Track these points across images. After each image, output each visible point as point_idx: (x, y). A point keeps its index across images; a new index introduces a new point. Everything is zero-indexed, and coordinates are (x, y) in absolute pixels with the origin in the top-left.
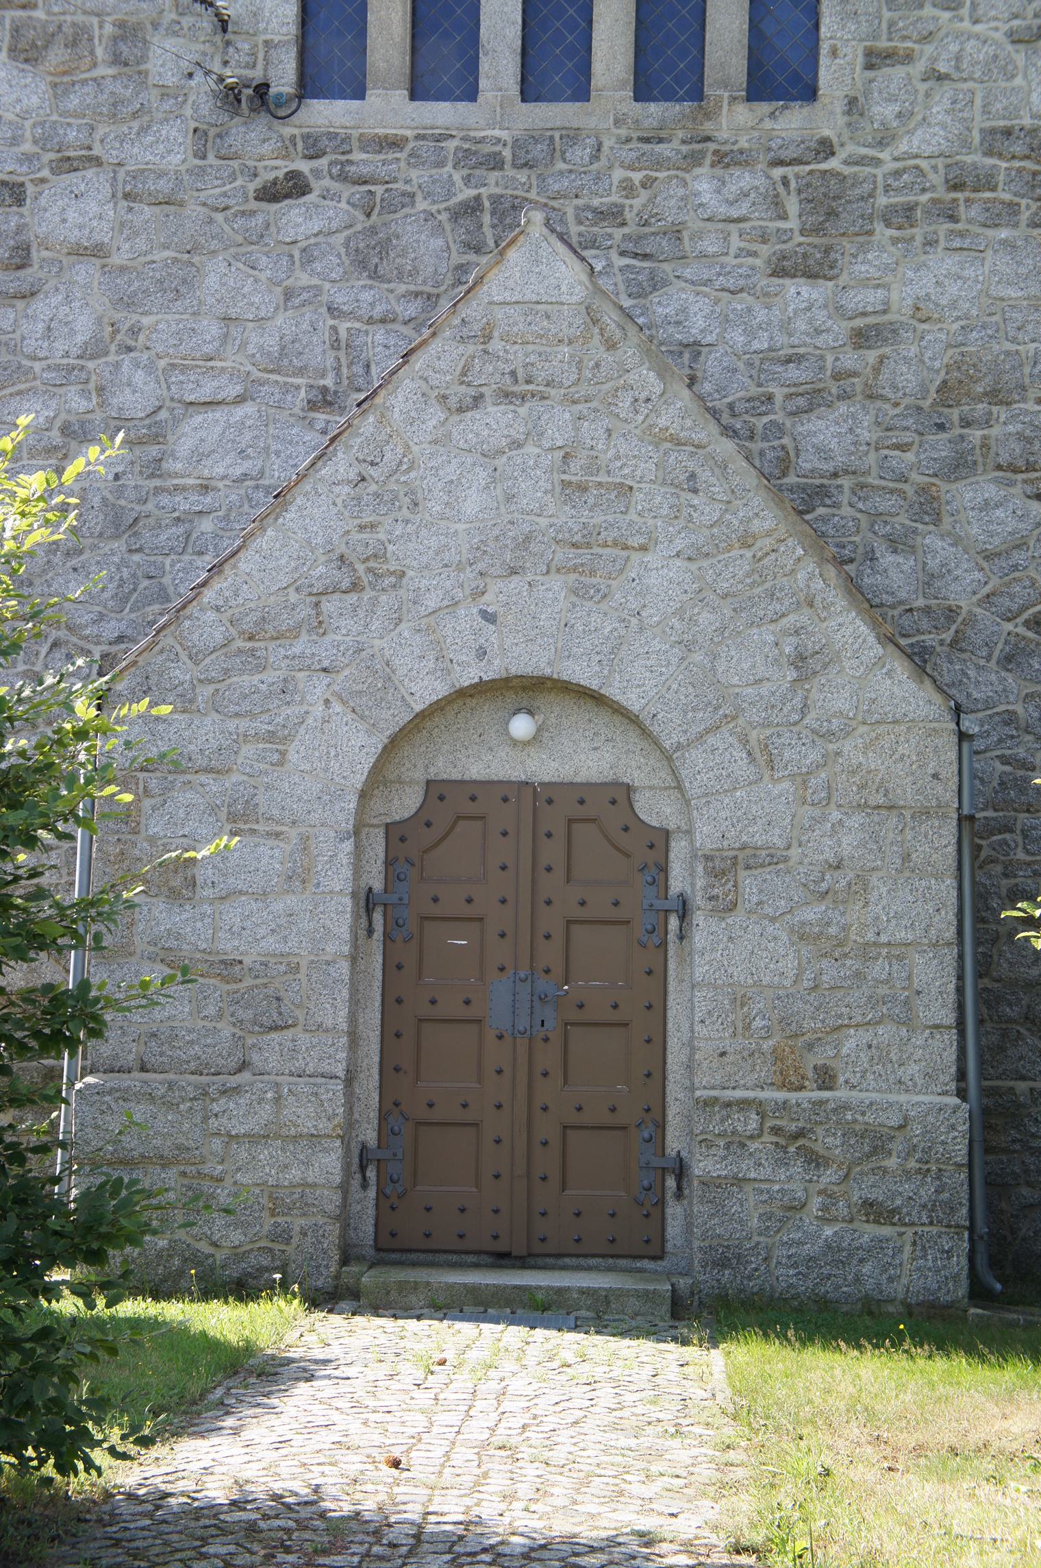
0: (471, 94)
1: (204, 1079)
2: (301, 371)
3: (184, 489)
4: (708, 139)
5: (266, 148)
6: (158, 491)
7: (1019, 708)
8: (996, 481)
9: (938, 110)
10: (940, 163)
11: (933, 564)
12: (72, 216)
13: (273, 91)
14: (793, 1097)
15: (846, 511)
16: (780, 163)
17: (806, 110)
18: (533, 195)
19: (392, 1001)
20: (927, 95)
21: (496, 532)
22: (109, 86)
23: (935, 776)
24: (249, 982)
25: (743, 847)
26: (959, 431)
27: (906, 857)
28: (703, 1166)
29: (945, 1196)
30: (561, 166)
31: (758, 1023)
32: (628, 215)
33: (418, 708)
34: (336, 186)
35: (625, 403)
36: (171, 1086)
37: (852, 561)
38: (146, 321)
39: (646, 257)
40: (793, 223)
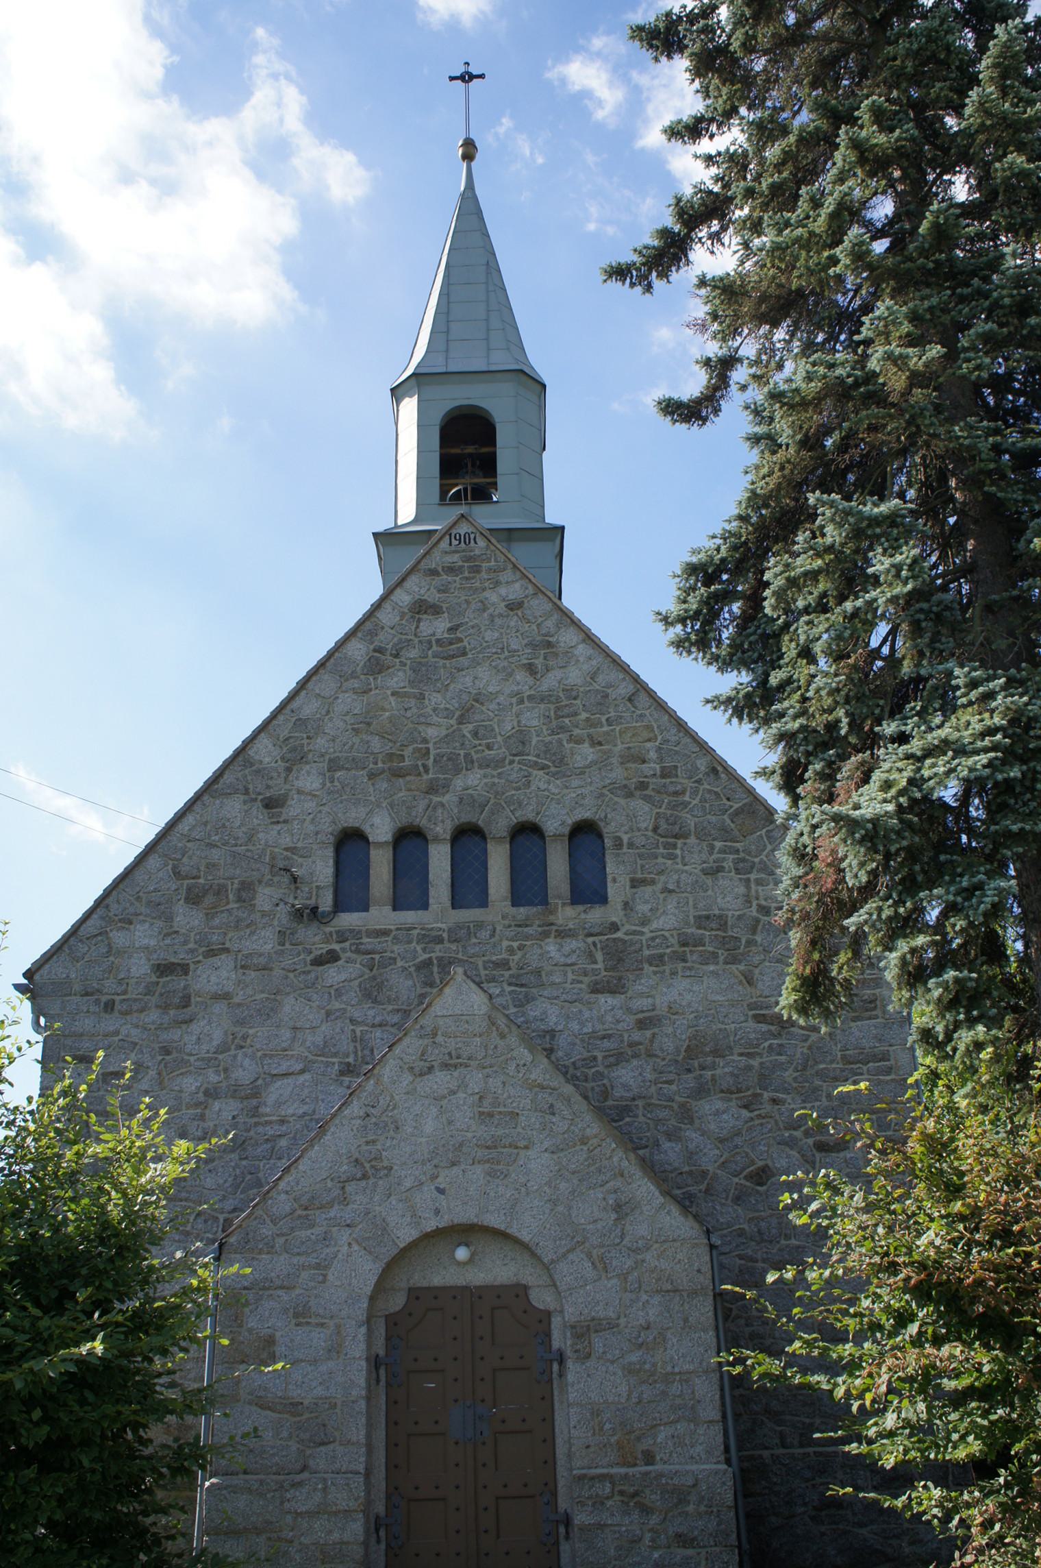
0: (425, 906)
1: (281, 1477)
2: (335, 1055)
3: (271, 1122)
4: (552, 924)
5: (317, 938)
6: (256, 1124)
7: (745, 1226)
8: (722, 1099)
9: (671, 906)
10: (675, 932)
11: (692, 1146)
12: (213, 979)
13: (320, 910)
14: (631, 1471)
15: (641, 1119)
16: (591, 935)
17: (603, 908)
18: (460, 956)
19: (392, 1423)
20: (664, 900)
21: (443, 1142)
22: (235, 913)
23: (699, 1271)
24: (306, 1416)
25: (593, 1319)
26: (698, 1072)
27: (686, 1320)
28: (581, 1518)
29: (723, 1526)
30: (474, 940)
31: (608, 1426)
32: (512, 964)
33: (402, 1246)
34: (354, 956)
35: (512, 1068)
36: (261, 1482)
37: (646, 1147)
38: (251, 1031)
39: (522, 985)
40: (600, 966)
